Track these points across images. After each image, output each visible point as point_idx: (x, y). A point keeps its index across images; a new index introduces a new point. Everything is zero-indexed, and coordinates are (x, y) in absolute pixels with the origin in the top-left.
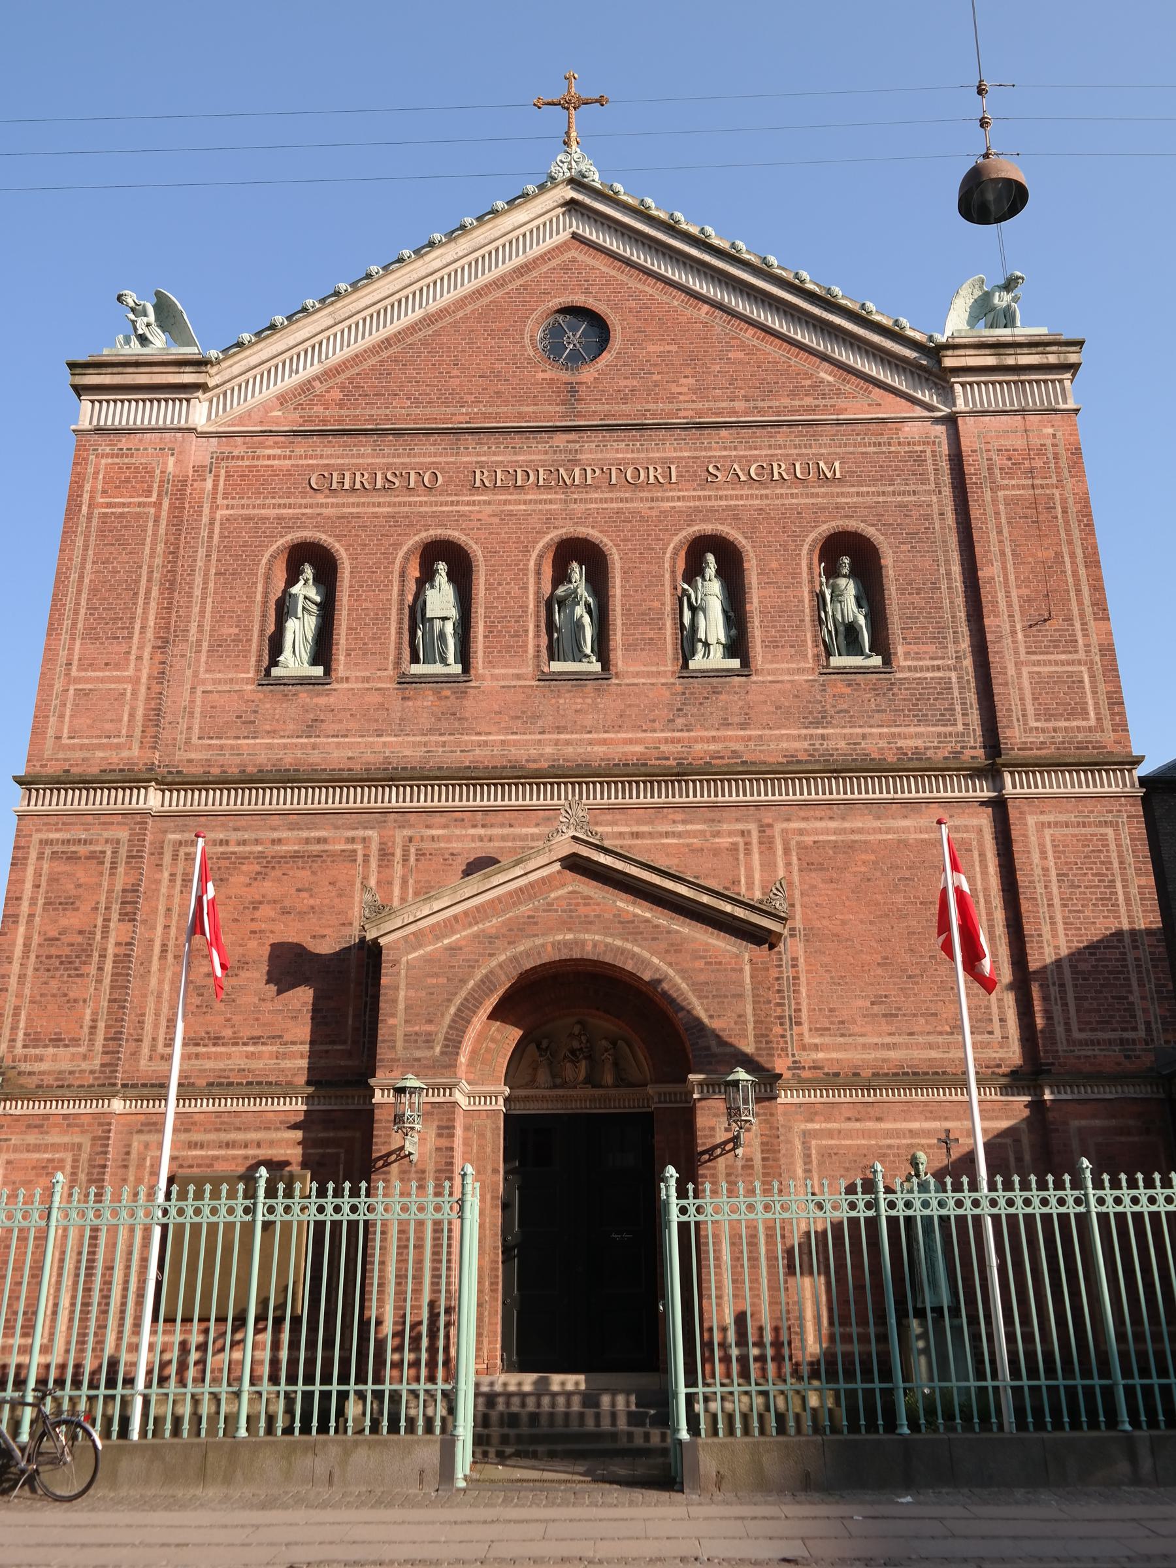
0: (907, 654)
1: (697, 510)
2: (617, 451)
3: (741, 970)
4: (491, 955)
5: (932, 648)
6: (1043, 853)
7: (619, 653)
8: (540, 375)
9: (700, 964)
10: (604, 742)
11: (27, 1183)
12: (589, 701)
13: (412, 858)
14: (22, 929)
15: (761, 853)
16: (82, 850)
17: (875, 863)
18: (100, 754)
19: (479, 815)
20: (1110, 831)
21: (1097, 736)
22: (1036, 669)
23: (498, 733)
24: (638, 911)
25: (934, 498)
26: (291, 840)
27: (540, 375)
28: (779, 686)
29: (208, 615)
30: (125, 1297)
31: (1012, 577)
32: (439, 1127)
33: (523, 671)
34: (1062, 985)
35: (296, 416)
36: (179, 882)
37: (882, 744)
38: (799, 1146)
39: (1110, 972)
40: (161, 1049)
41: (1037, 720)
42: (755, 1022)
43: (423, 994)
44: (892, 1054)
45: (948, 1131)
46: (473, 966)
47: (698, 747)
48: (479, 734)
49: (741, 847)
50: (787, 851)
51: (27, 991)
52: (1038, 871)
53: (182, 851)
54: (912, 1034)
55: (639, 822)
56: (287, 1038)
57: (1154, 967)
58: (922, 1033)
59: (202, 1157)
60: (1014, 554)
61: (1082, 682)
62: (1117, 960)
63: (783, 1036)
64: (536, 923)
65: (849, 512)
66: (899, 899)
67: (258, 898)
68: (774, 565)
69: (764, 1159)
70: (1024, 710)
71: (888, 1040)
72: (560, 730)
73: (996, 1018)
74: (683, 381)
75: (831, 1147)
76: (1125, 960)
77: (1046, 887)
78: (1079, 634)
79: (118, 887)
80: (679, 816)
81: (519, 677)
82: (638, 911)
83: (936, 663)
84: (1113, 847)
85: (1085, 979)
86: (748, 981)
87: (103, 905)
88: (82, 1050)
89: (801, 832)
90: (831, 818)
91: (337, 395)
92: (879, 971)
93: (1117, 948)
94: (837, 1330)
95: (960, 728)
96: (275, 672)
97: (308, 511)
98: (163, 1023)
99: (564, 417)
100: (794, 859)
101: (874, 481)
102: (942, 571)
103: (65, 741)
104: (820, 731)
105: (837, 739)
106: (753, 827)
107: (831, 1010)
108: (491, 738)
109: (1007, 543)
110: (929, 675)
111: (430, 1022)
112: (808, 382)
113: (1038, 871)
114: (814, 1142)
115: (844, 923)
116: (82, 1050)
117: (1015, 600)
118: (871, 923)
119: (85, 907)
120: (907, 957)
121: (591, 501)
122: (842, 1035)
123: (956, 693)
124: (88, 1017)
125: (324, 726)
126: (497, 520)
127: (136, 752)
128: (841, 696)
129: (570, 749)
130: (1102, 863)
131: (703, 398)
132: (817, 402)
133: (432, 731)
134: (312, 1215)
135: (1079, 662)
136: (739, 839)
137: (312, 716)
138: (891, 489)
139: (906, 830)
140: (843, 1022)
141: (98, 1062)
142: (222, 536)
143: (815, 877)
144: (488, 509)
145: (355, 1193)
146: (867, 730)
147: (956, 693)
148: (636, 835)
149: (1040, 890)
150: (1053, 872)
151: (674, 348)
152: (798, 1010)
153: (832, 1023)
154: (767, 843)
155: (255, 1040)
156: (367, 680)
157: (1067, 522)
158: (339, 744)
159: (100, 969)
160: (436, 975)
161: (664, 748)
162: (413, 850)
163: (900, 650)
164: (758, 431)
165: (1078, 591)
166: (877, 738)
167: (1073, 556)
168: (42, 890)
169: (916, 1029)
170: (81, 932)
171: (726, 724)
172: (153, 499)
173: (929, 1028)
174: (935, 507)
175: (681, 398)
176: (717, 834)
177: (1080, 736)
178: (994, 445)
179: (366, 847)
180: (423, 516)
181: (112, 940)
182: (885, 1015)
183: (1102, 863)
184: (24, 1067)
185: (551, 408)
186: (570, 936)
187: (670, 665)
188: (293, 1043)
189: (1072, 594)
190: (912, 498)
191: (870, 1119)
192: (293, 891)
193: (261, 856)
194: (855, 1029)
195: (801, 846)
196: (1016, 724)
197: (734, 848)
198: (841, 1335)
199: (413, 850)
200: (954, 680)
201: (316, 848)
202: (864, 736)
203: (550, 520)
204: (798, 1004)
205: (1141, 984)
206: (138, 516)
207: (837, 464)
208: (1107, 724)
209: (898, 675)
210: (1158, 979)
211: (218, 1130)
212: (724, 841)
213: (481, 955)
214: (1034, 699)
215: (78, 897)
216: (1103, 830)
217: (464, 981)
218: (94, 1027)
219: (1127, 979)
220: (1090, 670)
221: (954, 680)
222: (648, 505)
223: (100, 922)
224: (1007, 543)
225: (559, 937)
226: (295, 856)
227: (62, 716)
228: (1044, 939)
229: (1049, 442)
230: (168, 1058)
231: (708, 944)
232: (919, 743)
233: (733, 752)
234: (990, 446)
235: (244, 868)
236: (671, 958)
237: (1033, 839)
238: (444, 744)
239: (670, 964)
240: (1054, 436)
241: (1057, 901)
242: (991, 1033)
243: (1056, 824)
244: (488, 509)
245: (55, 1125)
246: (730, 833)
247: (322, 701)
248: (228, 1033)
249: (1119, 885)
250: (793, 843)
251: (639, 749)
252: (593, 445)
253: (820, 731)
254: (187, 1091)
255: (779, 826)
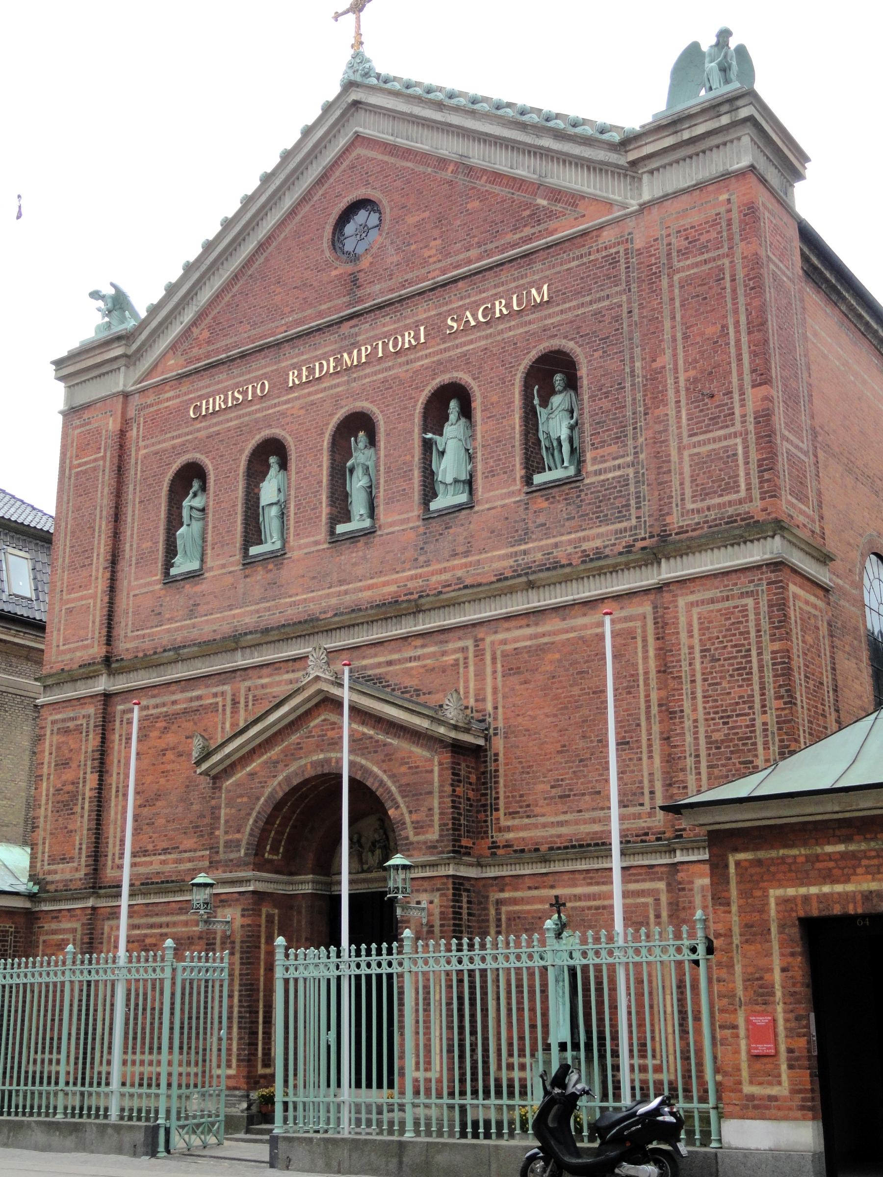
0: (594, 459)
1: (439, 363)
2: (384, 325)
3: (432, 771)
4: (275, 776)
5: (614, 448)
6: (690, 632)
7: (382, 507)
8: (334, 273)
9: (404, 769)
10: (369, 588)
11: (147, 951)
12: (361, 553)
13: (250, 704)
14: (45, 784)
15: (475, 664)
16: (71, 725)
17: (560, 661)
18: (78, 654)
19: (290, 664)
20: (750, 602)
21: (746, 507)
22: (696, 450)
23: (303, 594)
24: (366, 730)
25: (624, 298)
26: (181, 699)
27: (334, 273)
28: (493, 511)
29: (135, 536)
30: (103, 1029)
31: (681, 362)
32: (243, 910)
33: (318, 538)
34: (698, 756)
35: (181, 360)
36: (124, 741)
37: (570, 549)
38: (492, 912)
39: (740, 739)
40: (117, 861)
41: (694, 502)
42: (440, 814)
43: (233, 811)
44: (564, 830)
45: (557, 897)
46: (263, 784)
47: (434, 579)
48: (290, 596)
49: (461, 662)
50: (494, 659)
51: (48, 827)
52: (685, 650)
53: (126, 716)
54: (580, 811)
55: (392, 652)
56: (182, 848)
57: (780, 729)
58: (588, 810)
59: (139, 935)
60: (685, 337)
61: (735, 455)
62: (747, 726)
63: (486, 821)
64: (301, 748)
65: (554, 331)
66: (576, 691)
67: (164, 746)
68: (495, 399)
69: (442, 925)
70: (683, 494)
71: (563, 818)
72: (341, 582)
73: (646, 791)
74: (433, 243)
75: (515, 912)
76: (753, 725)
77: (690, 664)
78: (737, 405)
79: (90, 750)
80: (419, 642)
81: (316, 543)
82: (366, 730)
83: (617, 462)
84: (752, 617)
85: (718, 748)
86: (436, 779)
87: (82, 763)
88: (75, 864)
89: (504, 642)
90: (528, 626)
91: (206, 334)
92: (559, 758)
93: (749, 714)
94: (636, 1061)
95: (634, 522)
96: (434, 505)
97: (190, 437)
98: (118, 843)
99: (350, 305)
100: (499, 665)
101: (578, 294)
102: (628, 370)
103: (62, 648)
104: (523, 547)
105: (535, 550)
106: (469, 643)
107: (521, 796)
108: (298, 598)
109: (679, 328)
110: (610, 475)
111: (238, 831)
112: (528, 212)
113: (685, 650)
114: (771, 892)
115: (533, 718)
116: (75, 864)
117: (682, 383)
118: (555, 716)
119: (74, 765)
120: (581, 744)
121: (366, 376)
122: (528, 817)
123: (632, 489)
124: (77, 843)
125: (199, 608)
126: (302, 412)
127: (758, 504)
128: (541, 511)
129: (348, 597)
130: (741, 633)
131: (448, 255)
132: (533, 230)
133: (264, 599)
134: (672, 956)
135: (735, 435)
136: (459, 656)
137: (191, 602)
138: (588, 299)
139: (585, 627)
140: (528, 806)
141: (83, 873)
142: (142, 471)
143: (515, 680)
144: (297, 404)
145: (390, 952)
146: (558, 539)
147: (632, 489)
148: (390, 663)
149: (685, 667)
150: (697, 649)
151: (427, 214)
152: (497, 798)
153: (521, 807)
154: (479, 654)
155: (165, 851)
156: (223, 566)
157: (734, 291)
158: (207, 621)
159: (83, 808)
160: (241, 796)
161: (410, 584)
162: (251, 697)
163: (589, 456)
164: (487, 273)
165: (739, 359)
166: (566, 543)
167: (737, 323)
168: (53, 756)
169: (582, 806)
170: (73, 783)
171: (455, 555)
172: (725, 249)
173: (594, 804)
174: (625, 306)
175: (431, 260)
176: (444, 653)
177: (731, 511)
178: (674, 227)
179: (224, 699)
180: (257, 421)
181: (88, 788)
182: (560, 797)
183: (741, 633)
184: (49, 878)
185: (339, 301)
186: (321, 756)
187: (416, 511)
188: (185, 851)
189: (734, 365)
190: (606, 303)
191: (545, 887)
192: (183, 739)
193: (166, 715)
194: (537, 810)
195: (505, 655)
196: (675, 509)
197: (456, 664)
198: (640, 1066)
199: (251, 697)
200: (631, 475)
201: (196, 704)
202: (556, 545)
203: (337, 399)
204: (497, 793)
205: (766, 748)
206: (95, 469)
207: (545, 287)
208: (756, 494)
209: (587, 481)
210: (782, 741)
211: (147, 916)
212: (449, 659)
213: (268, 777)
214: (692, 481)
215: (70, 759)
216: (744, 601)
217: (258, 799)
218: (80, 849)
219: (755, 744)
220: (745, 441)
221: (631, 475)
222: (405, 368)
223: (81, 776)
224: (679, 328)
225: (315, 758)
226: (185, 712)
227: (59, 630)
228: (685, 714)
229: (722, 210)
230: (120, 867)
231: (411, 752)
232: (598, 543)
233: (459, 579)
234: (671, 231)
235: (158, 725)
236: (385, 766)
237: (683, 620)
238: (269, 609)
239: (385, 771)
240: (729, 201)
241: (699, 677)
242: (642, 805)
243: (703, 602)
244: (297, 404)
245: (64, 917)
246: (455, 651)
247: (199, 589)
248: (150, 847)
249: (754, 653)
250: (499, 653)
251: (393, 588)
252: (367, 325)
253: (523, 547)
254: (601, 847)
255: (489, 639)
